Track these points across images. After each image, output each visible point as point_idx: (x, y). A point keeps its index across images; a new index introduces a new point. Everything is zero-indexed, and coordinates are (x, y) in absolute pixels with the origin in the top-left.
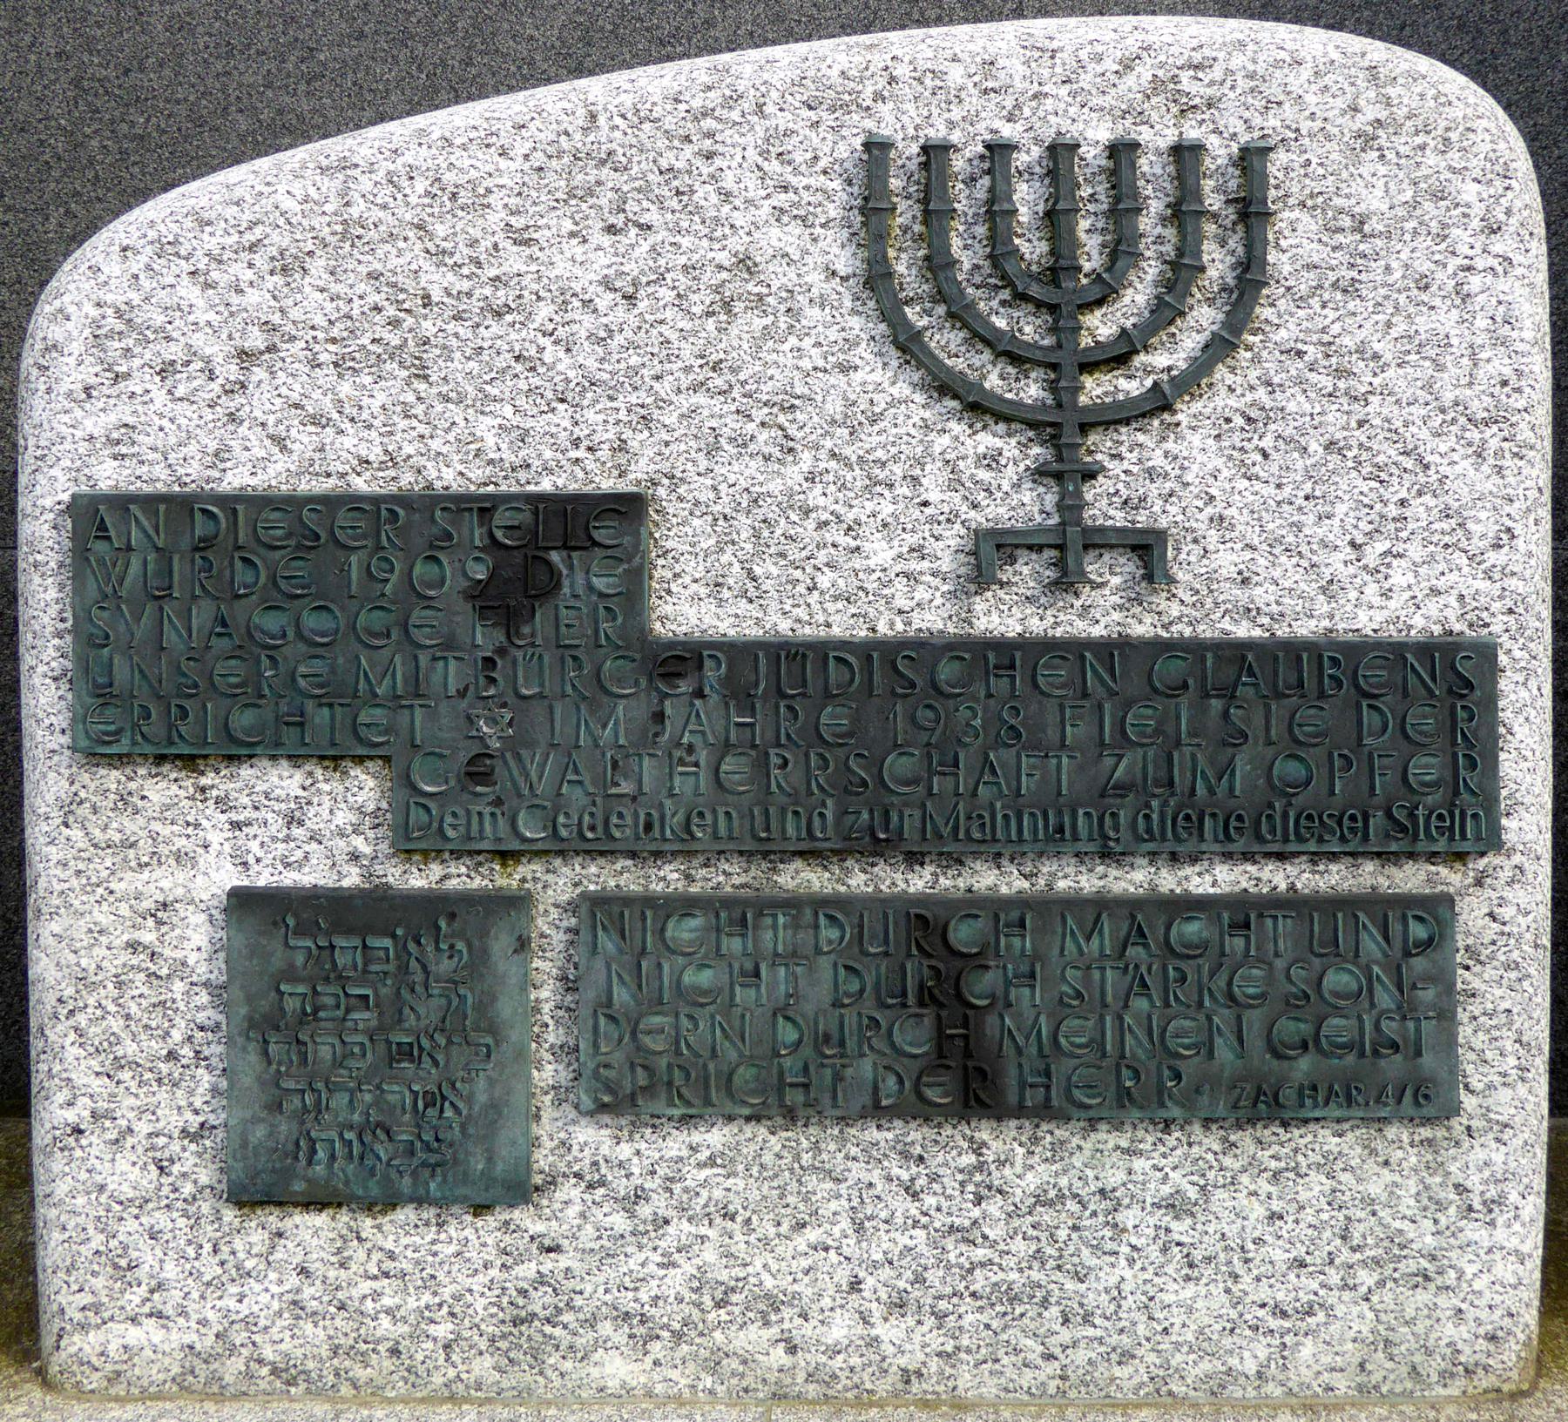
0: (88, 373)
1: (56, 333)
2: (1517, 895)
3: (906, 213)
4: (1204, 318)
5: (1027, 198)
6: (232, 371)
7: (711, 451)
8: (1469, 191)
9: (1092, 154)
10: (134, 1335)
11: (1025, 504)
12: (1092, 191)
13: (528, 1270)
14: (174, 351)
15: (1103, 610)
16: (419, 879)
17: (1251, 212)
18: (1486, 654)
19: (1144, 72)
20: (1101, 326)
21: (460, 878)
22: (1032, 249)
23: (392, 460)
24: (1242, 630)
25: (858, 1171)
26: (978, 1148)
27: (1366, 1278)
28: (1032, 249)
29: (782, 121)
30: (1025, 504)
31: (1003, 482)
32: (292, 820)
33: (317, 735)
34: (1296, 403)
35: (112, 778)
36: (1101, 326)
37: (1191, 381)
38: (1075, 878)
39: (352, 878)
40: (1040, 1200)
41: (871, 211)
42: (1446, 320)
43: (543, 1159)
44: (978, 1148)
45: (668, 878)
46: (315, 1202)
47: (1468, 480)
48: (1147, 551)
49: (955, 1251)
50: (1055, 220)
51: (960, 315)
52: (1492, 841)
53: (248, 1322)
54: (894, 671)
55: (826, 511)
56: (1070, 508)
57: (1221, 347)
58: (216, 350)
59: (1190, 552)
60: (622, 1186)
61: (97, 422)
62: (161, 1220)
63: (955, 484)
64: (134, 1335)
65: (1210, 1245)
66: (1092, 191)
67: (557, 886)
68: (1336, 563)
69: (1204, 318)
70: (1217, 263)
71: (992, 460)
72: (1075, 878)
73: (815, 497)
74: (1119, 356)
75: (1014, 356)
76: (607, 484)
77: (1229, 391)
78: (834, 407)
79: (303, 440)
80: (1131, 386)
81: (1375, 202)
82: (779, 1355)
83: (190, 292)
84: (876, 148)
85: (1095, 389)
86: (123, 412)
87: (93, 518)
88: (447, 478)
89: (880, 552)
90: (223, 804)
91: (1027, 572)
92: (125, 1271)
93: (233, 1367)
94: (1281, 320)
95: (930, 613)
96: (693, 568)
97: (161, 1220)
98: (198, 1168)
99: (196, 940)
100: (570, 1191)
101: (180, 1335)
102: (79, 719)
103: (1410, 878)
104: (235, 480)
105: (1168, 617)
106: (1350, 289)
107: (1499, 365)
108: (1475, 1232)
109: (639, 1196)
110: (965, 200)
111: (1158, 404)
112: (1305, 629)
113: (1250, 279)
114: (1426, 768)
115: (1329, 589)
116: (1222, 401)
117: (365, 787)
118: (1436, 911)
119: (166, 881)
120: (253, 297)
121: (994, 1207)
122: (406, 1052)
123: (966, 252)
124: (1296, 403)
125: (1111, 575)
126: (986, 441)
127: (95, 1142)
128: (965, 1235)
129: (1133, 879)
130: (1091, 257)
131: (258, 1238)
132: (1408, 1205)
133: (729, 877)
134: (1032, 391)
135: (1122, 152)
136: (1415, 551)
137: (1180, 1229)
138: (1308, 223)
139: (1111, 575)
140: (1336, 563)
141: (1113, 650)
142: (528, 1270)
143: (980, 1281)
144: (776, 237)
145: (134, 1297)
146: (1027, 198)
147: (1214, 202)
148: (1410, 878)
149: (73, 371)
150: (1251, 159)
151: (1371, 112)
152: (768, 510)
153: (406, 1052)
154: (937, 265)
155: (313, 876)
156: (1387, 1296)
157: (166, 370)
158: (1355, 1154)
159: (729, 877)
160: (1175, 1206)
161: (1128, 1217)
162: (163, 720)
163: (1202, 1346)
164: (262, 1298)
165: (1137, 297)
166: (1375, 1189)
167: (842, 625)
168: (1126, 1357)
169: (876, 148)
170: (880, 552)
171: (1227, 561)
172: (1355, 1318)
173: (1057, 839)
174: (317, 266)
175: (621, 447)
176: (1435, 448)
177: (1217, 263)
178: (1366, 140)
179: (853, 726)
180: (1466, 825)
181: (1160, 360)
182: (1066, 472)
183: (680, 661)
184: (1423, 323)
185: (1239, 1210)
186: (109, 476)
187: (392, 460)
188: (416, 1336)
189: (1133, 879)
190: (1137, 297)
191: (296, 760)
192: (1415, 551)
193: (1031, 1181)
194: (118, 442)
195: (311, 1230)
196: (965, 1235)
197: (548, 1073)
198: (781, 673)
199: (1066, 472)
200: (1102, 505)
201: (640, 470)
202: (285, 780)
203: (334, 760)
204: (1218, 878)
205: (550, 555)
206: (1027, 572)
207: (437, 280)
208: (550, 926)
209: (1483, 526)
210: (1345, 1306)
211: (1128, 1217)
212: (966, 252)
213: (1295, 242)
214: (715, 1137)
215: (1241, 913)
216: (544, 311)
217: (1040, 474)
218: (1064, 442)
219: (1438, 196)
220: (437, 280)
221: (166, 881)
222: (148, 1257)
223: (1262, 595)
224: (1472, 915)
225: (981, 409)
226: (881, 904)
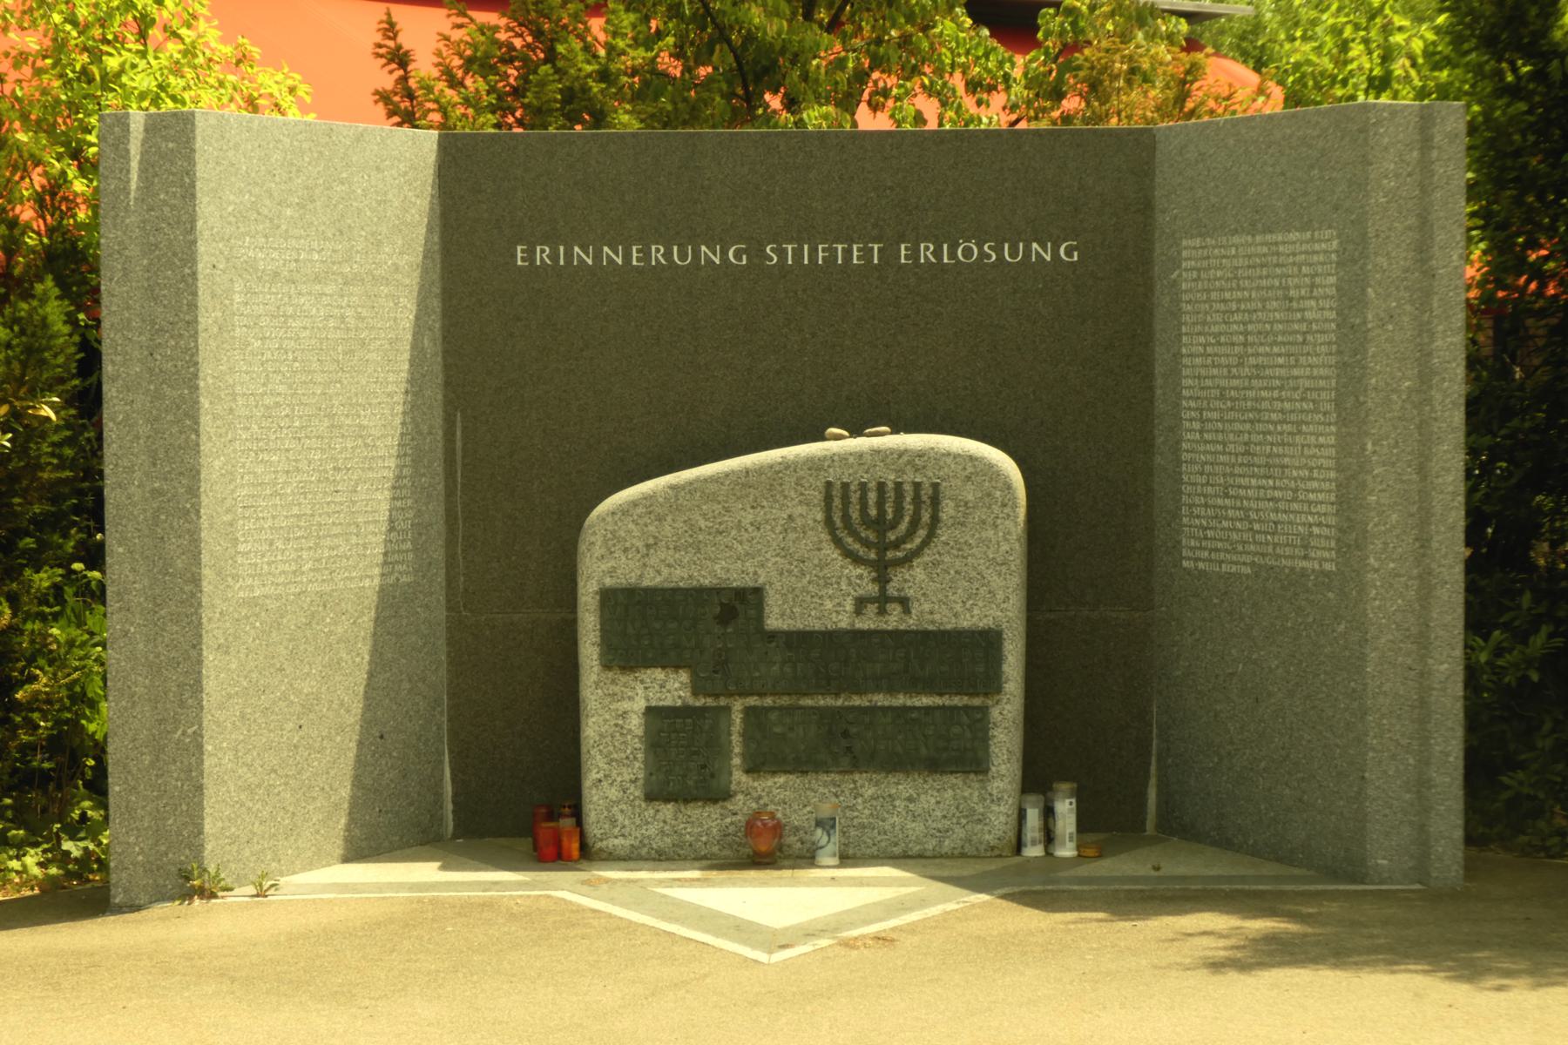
0: (603, 551)
1: (593, 539)
2: (1008, 707)
3: (837, 502)
4: (922, 533)
5: (872, 497)
6: (644, 550)
7: (781, 574)
8: (998, 493)
9: (890, 485)
10: (616, 842)
11: (872, 589)
12: (891, 494)
13: (728, 820)
14: (628, 544)
15: (894, 620)
16: (700, 702)
17: (935, 501)
18: (606, 666)
19: (905, 458)
20: (892, 536)
21: (710, 702)
22: (873, 512)
23: (690, 577)
24: (931, 628)
25: (821, 790)
26: (855, 782)
27: (964, 821)
28: (873, 512)
29: (801, 473)
30: (872, 589)
31: (861, 580)
32: (662, 686)
33: (667, 659)
34: (947, 559)
35: (610, 674)
36: (892, 536)
37: (917, 553)
38: (881, 700)
39: (679, 703)
40: (873, 798)
41: (828, 499)
42: (991, 533)
43: (733, 787)
44: (855, 782)
45: (768, 701)
46: (667, 800)
47: (996, 582)
48: (904, 602)
49: (848, 813)
50: (880, 504)
51: (854, 534)
52: (999, 690)
53: (649, 837)
54: (831, 638)
55: (816, 593)
56: (883, 590)
57: (926, 543)
58: (640, 544)
59: (916, 604)
60: (755, 795)
61: (604, 567)
62: (624, 807)
63: (850, 584)
64: (616, 842)
65: (920, 811)
66: (891, 494)
67: (738, 705)
68: (958, 607)
69: (922, 533)
70: (926, 517)
71: (860, 577)
72: (881, 700)
73: (810, 588)
74: (896, 545)
75: (866, 543)
76: (751, 584)
77: (927, 558)
78: (816, 561)
79: (665, 571)
80: (900, 554)
81: (970, 497)
82: (799, 845)
83: (631, 526)
84: (829, 485)
85: (890, 555)
86: (612, 563)
87: (608, 597)
88: (706, 582)
89: (829, 605)
90: (642, 682)
91: (872, 609)
92: (613, 822)
93: (644, 851)
94: (944, 535)
95: (844, 623)
96: (776, 610)
97: (624, 807)
98: (636, 792)
99: (636, 723)
100: (740, 796)
101: (627, 843)
102: (602, 655)
103: (977, 702)
104: (646, 583)
105: (911, 623)
106: (963, 524)
107: (1005, 547)
108: (995, 808)
109: (760, 797)
110: (855, 497)
111: (907, 560)
112: (949, 627)
113: (935, 519)
114: (980, 669)
115: (956, 615)
116: (926, 559)
117: (684, 676)
118: (984, 710)
119: (626, 705)
120: (651, 528)
121: (860, 800)
122: (695, 753)
123: (855, 514)
124: (947, 559)
125: (895, 610)
126: (859, 571)
127: (605, 784)
128: (852, 808)
129: (901, 700)
130: (890, 516)
131: (652, 812)
132: (975, 799)
133: (785, 701)
134: (873, 556)
135: (898, 486)
136: (981, 604)
137: (911, 806)
138: (951, 504)
139: (895, 610)
140: (958, 607)
141: (896, 634)
142: (728, 820)
143: (856, 822)
144: (800, 510)
145: (616, 831)
146: (872, 497)
147: (924, 498)
148: (977, 702)
149: (598, 551)
150: (935, 486)
151: (970, 470)
152: (797, 592)
153: (695, 753)
154: (846, 517)
155: (668, 703)
156: (969, 827)
157: (626, 550)
158: (961, 784)
159: (785, 701)
160: (910, 799)
161: (897, 803)
162: (625, 655)
163: (918, 842)
164: (652, 830)
165: (903, 526)
166: (966, 794)
167: (817, 626)
168: (896, 844)
169: (829, 485)
170: (829, 605)
171: (927, 607)
172: (960, 833)
173: (878, 689)
174: (669, 518)
175: (755, 573)
176: (987, 573)
177: (926, 517)
178: (968, 478)
179: (824, 655)
180: (991, 683)
181: (908, 546)
182: (882, 580)
183: (773, 635)
184: (984, 535)
185: (927, 801)
186: (608, 582)
187: (690, 577)
188: (697, 840)
189: (901, 700)
190: (903, 526)
191: (663, 667)
192: (981, 604)
193: (870, 792)
194: (612, 572)
195: (668, 810)
196: (852, 808)
197: (737, 761)
198: (799, 641)
199: (882, 580)
200: (892, 590)
201: (761, 580)
202: (659, 674)
203: (677, 667)
204: (925, 701)
205: (738, 605)
206: (872, 609)
207: (702, 523)
208: (737, 718)
209: (1000, 596)
210: (957, 829)
211: (897, 803)
212: (855, 514)
213: (948, 510)
214: (781, 779)
215: (928, 710)
216: (734, 532)
217: (874, 580)
218: (882, 570)
219: (989, 495)
220: (702, 523)
221: (626, 705)
222: (620, 818)
223: (937, 617)
224: (995, 713)
225: (857, 560)
226: (827, 708)
